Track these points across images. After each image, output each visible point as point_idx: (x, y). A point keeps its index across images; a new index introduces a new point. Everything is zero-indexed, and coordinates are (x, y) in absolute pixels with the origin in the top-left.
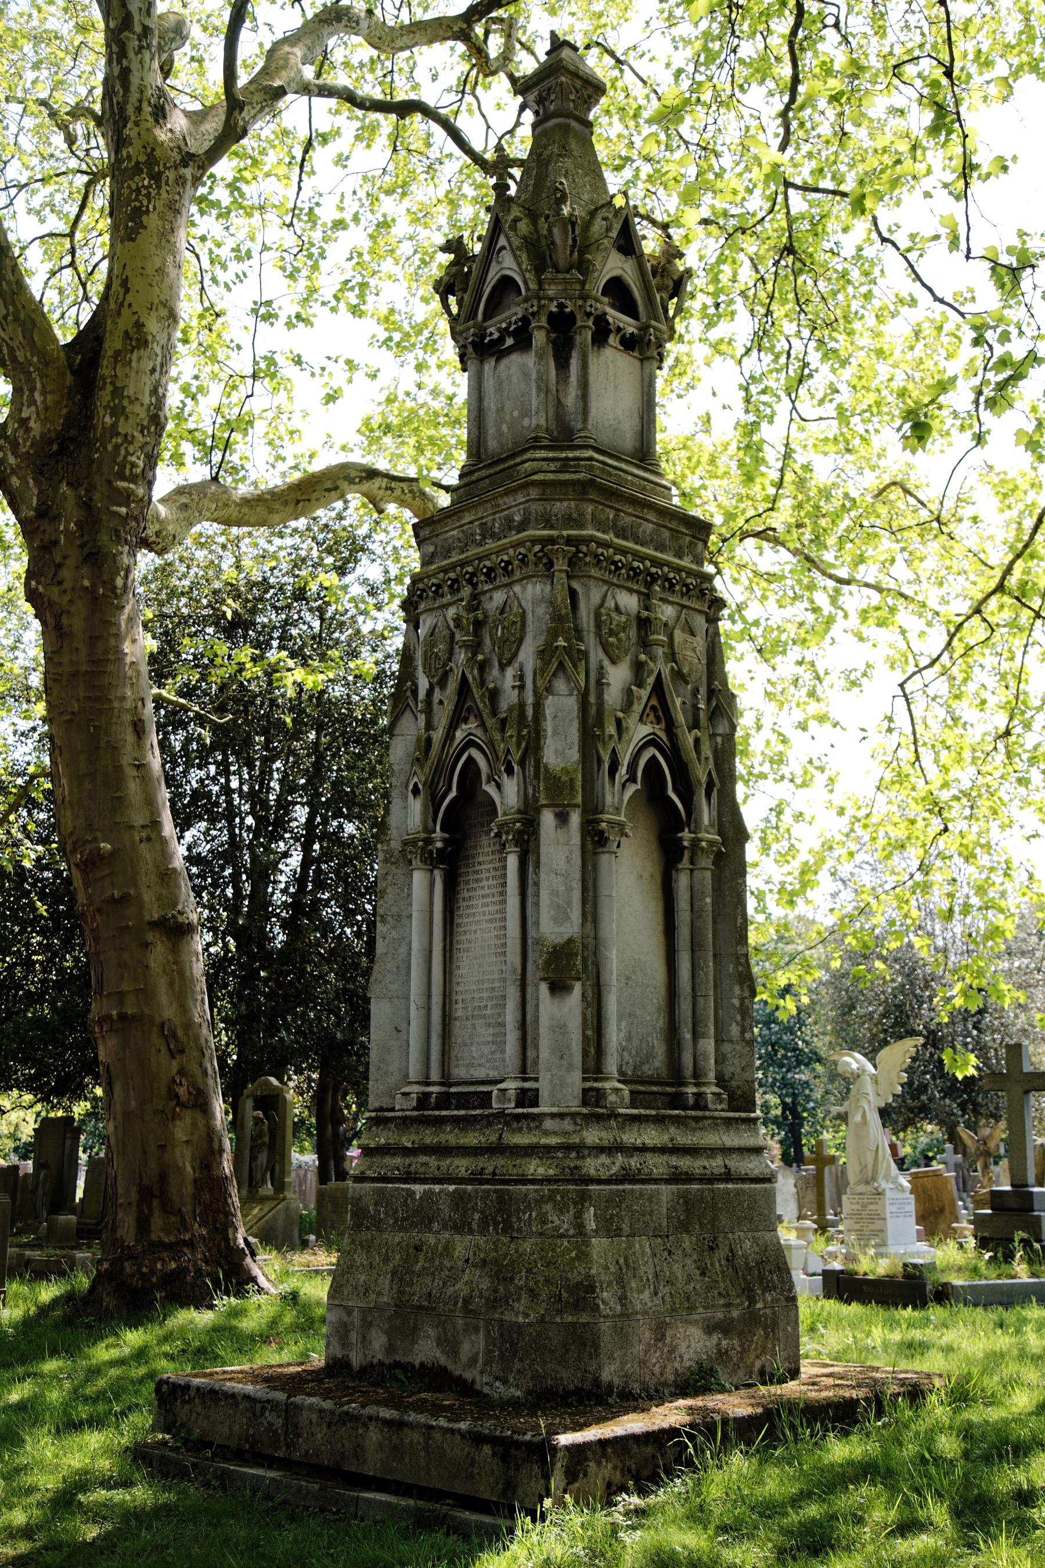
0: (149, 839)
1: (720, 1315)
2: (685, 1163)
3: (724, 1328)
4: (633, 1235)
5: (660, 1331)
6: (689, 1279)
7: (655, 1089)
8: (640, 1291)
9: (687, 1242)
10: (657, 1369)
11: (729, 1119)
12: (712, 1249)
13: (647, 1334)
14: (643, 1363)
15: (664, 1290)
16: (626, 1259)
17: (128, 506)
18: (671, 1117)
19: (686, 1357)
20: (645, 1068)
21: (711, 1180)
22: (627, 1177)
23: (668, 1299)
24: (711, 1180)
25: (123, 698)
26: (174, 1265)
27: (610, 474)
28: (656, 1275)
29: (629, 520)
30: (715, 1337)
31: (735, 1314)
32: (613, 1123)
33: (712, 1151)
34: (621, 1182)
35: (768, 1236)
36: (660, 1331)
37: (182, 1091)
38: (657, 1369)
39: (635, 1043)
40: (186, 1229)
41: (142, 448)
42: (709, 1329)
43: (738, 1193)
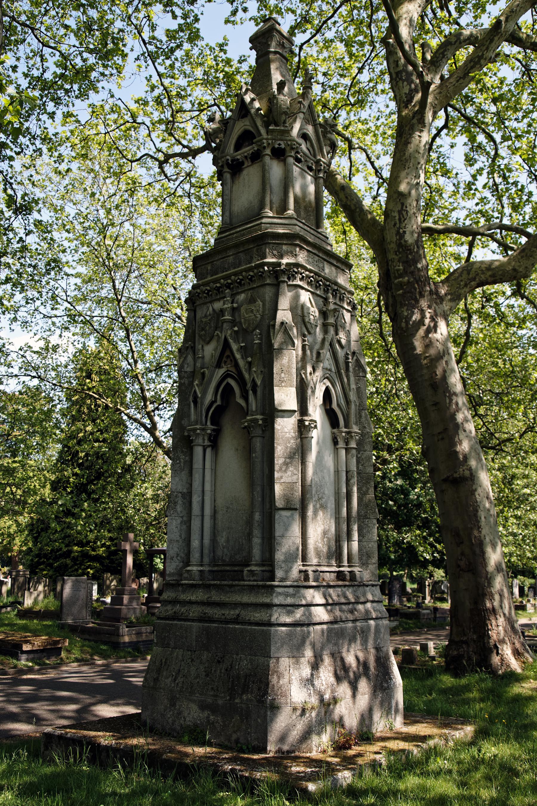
0: (443, 439)
2: (210, 611)
3: (213, 709)
4: (175, 648)
5: (173, 701)
6: (197, 677)
7: (228, 568)
9: (205, 656)
12: (219, 662)
13: (166, 701)
15: (180, 680)
16: (166, 659)
17: (402, 289)
18: (214, 585)
19: (188, 719)
20: (237, 557)
21: (227, 622)
23: (180, 685)
24: (227, 622)
26: (455, 653)
27: (232, 238)
29: (218, 263)
30: (206, 713)
31: (220, 702)
34: (174, 619)
36: (173, 701)
38: (170, 720)
40: (465, 635)
41: (399, 261)
42: (203, 707)
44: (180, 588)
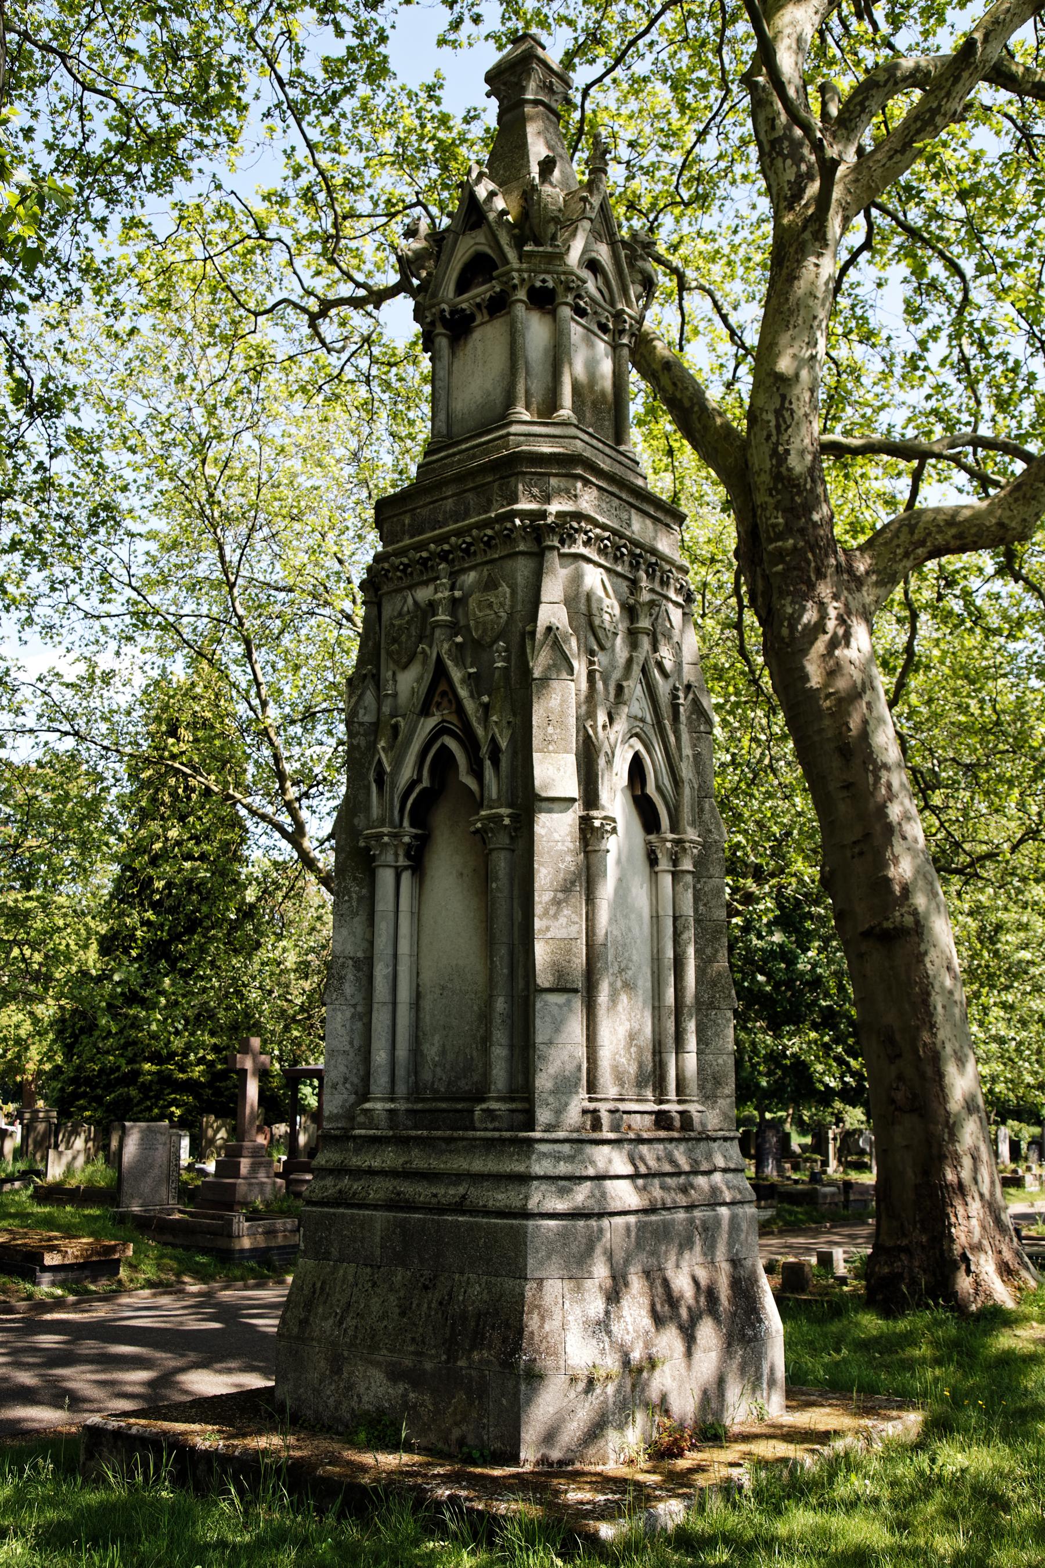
1: (408, 1362)
2: (409, 1189)
3: (414, 1378)
4: (341, 1260)
5: (336, 1364)
6: (384, 1316)
8: (325, 1318)
9: (400, 1276)
10: (331, 1401)
11: (493, 1140)
12: (426, 1288)
13: (322, 1364)
14: (317, 1392)
15: (350, 1322)
16: (324, 1283)
17: (783, 562)
18: (417, 1138)
19: (365, 1399)
20: (462, 1083)
21: (442, 1210)
22: (341, 1200)
23: (350, 1333)
24: (442, 1210)
25: (821, 731)
28: (349, 1304)
30: (401, 1388)
31: (428, 1366)
32: (351, 1145)
33: (458, 1177)
34: (338, 1205)
35: (509, 1283)
36: (336, 1364)
37: (899, 1096)
38: (331, 1401)
39: (450, 1056)
42: (395, 1375)
43: (471, 1227)
44: (351, 1145)
